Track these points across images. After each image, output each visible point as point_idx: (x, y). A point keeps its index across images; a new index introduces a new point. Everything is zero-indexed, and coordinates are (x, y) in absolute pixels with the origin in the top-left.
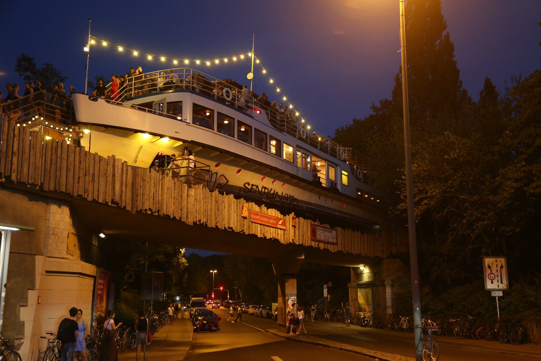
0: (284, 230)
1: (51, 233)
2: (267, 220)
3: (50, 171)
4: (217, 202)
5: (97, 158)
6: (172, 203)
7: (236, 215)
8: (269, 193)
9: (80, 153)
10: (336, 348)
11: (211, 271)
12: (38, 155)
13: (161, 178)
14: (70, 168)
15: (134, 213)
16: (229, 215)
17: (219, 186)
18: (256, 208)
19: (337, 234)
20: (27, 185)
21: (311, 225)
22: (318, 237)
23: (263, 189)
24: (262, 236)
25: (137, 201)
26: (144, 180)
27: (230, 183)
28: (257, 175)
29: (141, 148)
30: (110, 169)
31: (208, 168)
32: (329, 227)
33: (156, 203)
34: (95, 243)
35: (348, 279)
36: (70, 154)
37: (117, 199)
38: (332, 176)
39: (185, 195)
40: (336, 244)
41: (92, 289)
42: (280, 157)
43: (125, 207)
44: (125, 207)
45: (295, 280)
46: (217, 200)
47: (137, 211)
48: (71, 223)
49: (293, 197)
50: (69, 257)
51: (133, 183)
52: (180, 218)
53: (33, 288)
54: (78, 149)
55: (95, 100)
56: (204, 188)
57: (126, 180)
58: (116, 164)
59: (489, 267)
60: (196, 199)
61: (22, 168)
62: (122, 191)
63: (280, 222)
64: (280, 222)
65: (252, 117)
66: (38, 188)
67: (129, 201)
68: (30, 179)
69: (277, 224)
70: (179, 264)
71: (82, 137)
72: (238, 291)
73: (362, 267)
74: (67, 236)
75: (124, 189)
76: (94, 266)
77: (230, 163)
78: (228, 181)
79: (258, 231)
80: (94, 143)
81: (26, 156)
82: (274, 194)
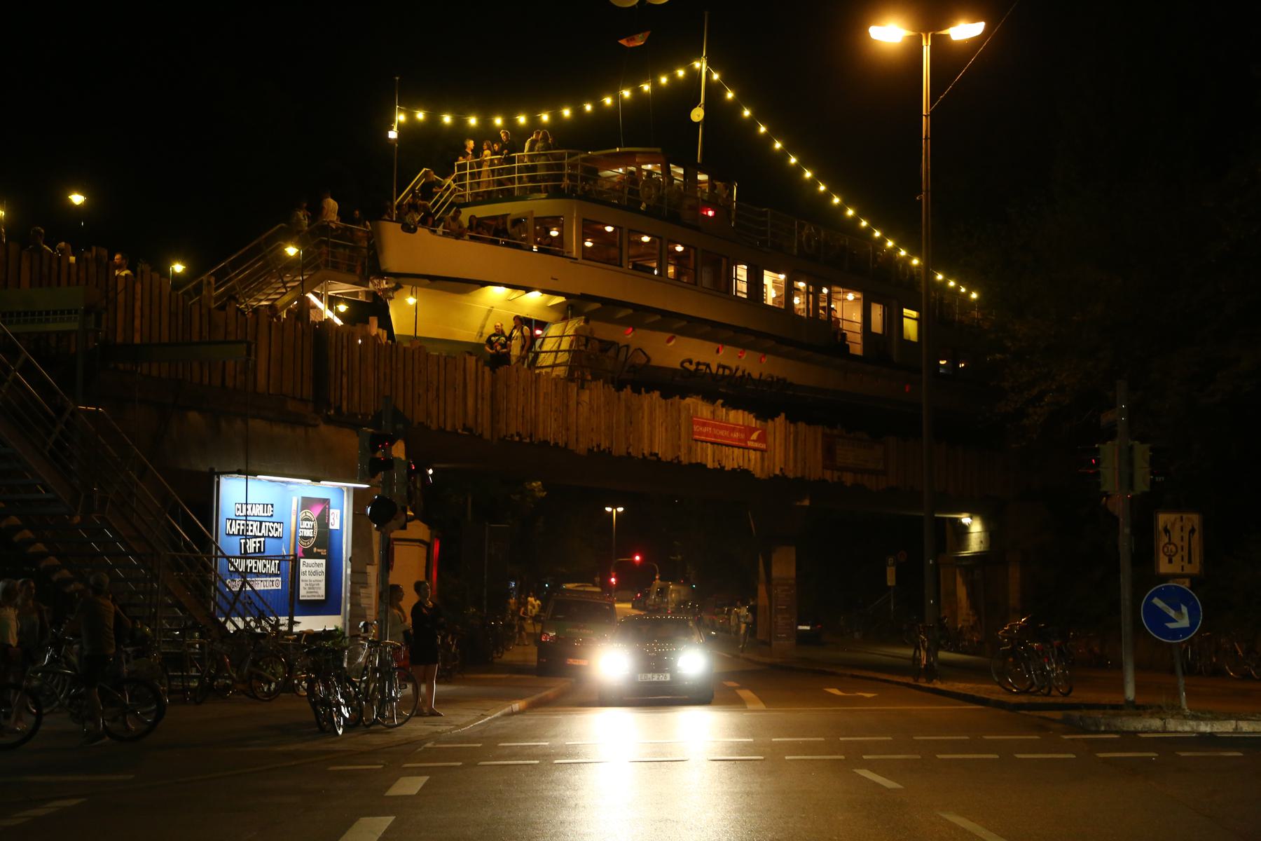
0: (762, 451)
2: (726, 433)
8: (732, 376)
11: (608, 509)
16: (651, 433)
18: (703, 410)
23: (721, 371)
27: (654, 362)
28: (708, 343)
29: (490, 311)
39: (572, 404)
43: (481, 435)
44: (481, 435)
49: (785, 380)
59: (1166, 531)
63: (754, 436)
64: (754, 436)
69: (747, 439)
77: (654, 327)
78: (649, 360)
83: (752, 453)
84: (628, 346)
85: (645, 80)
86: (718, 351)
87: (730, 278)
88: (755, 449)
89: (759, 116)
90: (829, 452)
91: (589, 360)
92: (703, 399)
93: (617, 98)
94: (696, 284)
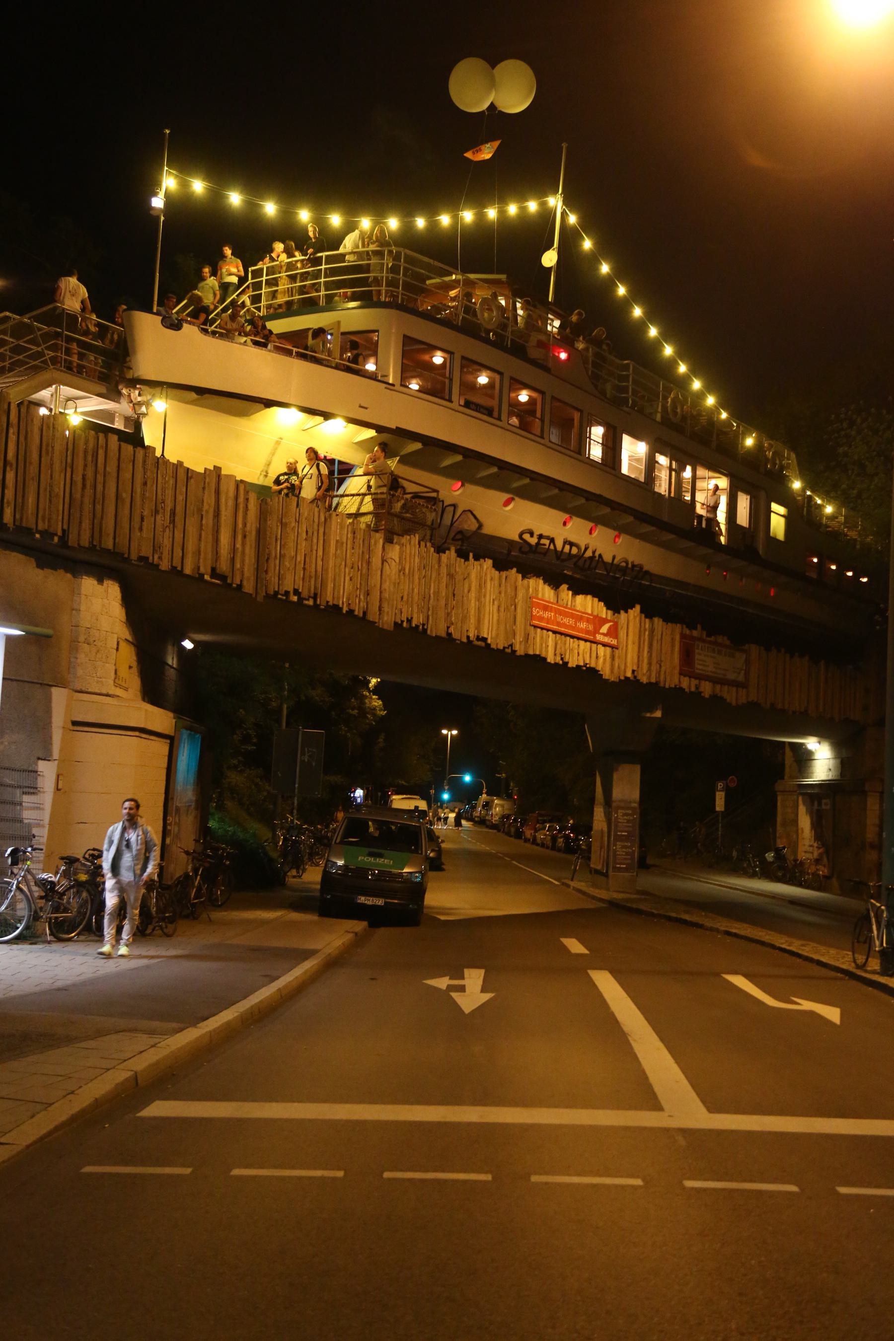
0: (612, 647)
1: (82, 638)
2: (572, 622)
3: (82, 502)
4: (451, 576)
5: (181, 475)
6: (347, 578)
7: (496, 607)
8: (580, 557)
9: (144, 462)
10: (717, 931)
11: (444, 732)
12: (57, 466)
13: (323, 519)
14: (124, 495)
15: (260, 599)
17: (459, 537)
18: (546, 592)
19: (747, 662)
20: (34, 534)
21: (683, 636)
22: (699, 667)
23: (567, 547)
24: (558, 660)
25: (266, 572)
26: (283, 525)
27: (486, 530)
29: (278, 443)
30: (209, 499)
31: (434, 495)
32: (728, 642)
33: (310, 577)
34: (172, 660)
35: (779, 772)
36: (122, 465)
37: (224, 566)
38: (743, 517)
39: (376, 561)
40: (744, 685)
41: (165, 765)
42: (614, 468)
43: (240, 586)
45: (638, 768)
46: (452, 571)
47: (267, 596)
48: (124, 618)
49: (641, 567)
50: (119, 692)
51: (259, 531)
52: (365, 613)
53: (47, 757)
54: (140, 452)
55: (176, 326)
56: (423, 543)
57: (245, 525)
58: (223, 487)
60: (402, 570)
61: (23, 496)
62: (234, 550)
63: (605, 629)
64: (605, 629)
65: (546, 369)
66: (56, 539)
67: (249, 572)
68: (40, 521)
69: (596, 631)
70: (363, 711)
71: (145, 415)
72: (508, 785)
73: (811, 743)
74: (115, 647)
75: (239, 545)
76: (171, 715)
77: (488, 483)
78: (481, 526)
79: (549, 648)
80: (171, 431)
81: (33, 470)
82: (592, 558)
83: (601, 649)
84: (455, 506)
85: (491, 204)
86: (565, 524)
87: (583, 440)
88: (604, 645)
89: (620, 273)
90: (687, 656)
91: (400, 513)
92: (545, 581)
93: (456, 218)
94: (542, 437)
